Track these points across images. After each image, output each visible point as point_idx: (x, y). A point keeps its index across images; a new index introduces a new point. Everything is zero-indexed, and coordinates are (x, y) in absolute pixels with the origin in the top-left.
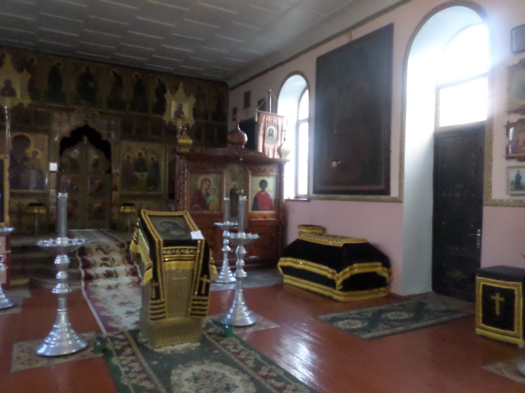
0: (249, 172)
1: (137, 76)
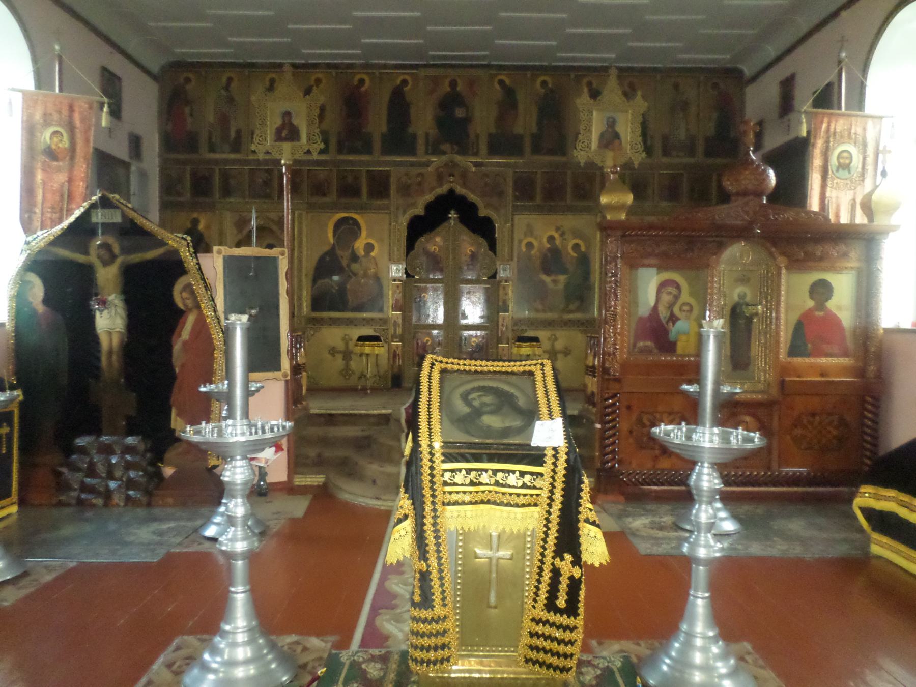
0: (782, 261)
1: (544, 83)
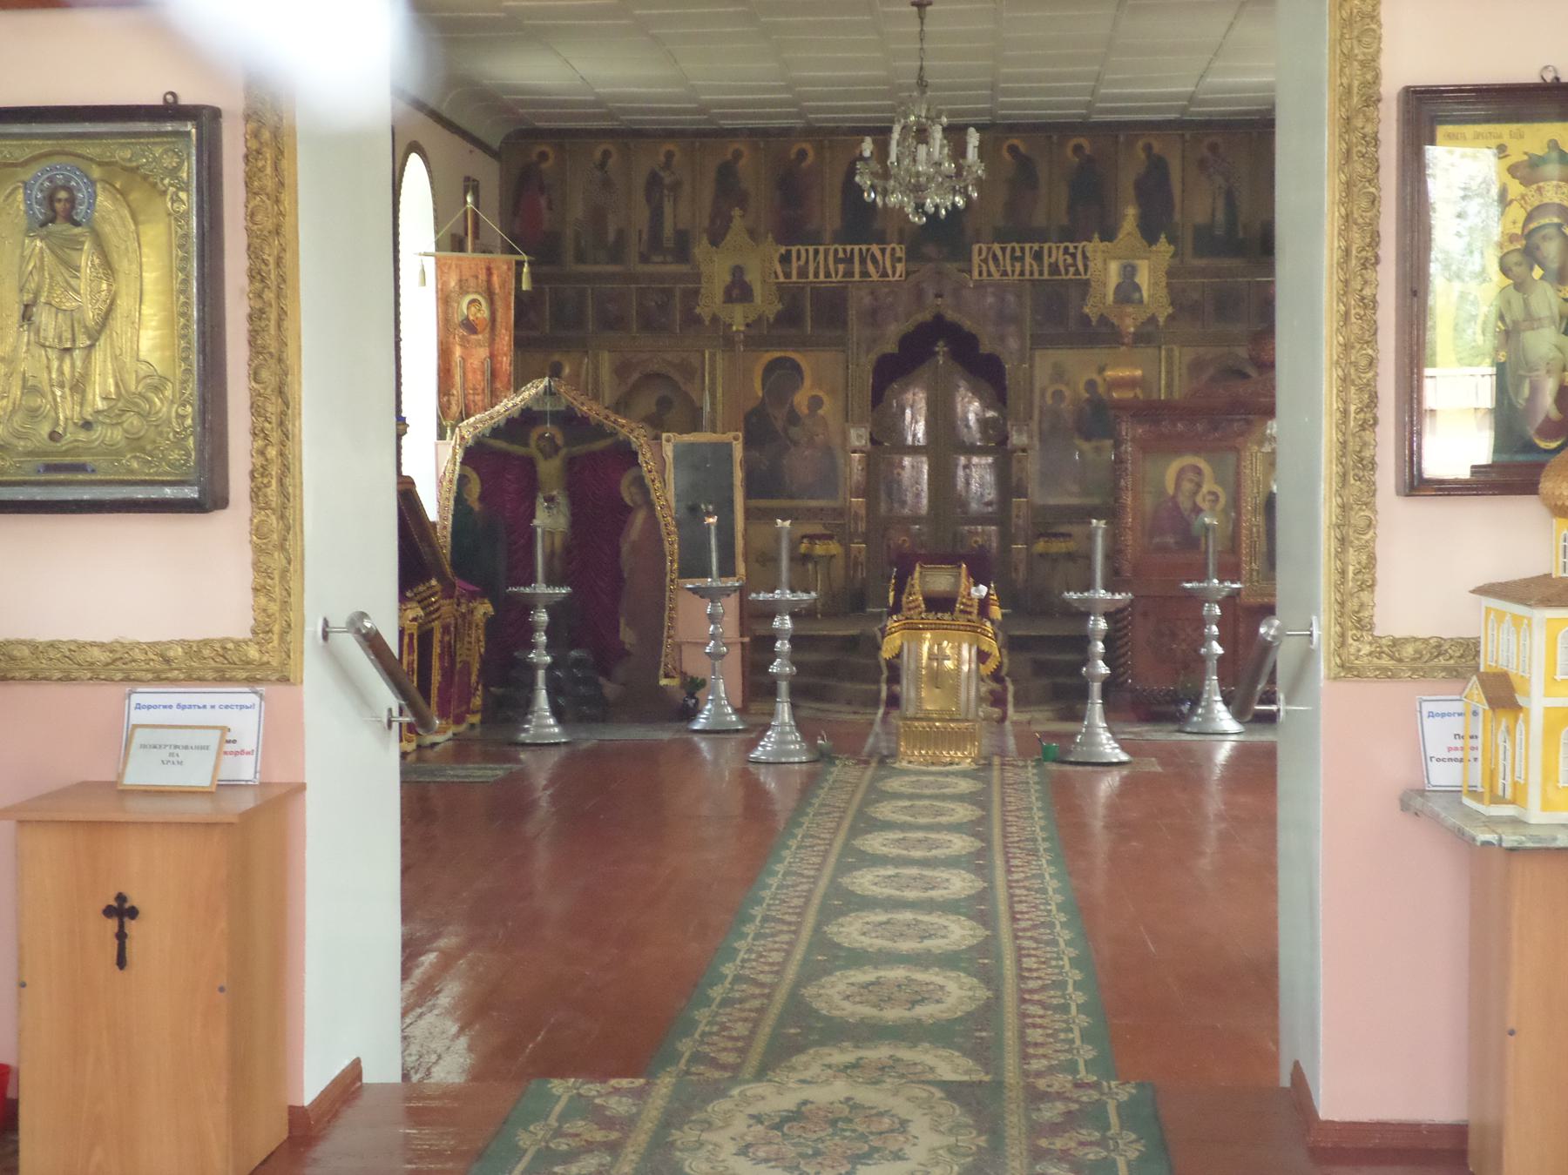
1: (1078, 149)
